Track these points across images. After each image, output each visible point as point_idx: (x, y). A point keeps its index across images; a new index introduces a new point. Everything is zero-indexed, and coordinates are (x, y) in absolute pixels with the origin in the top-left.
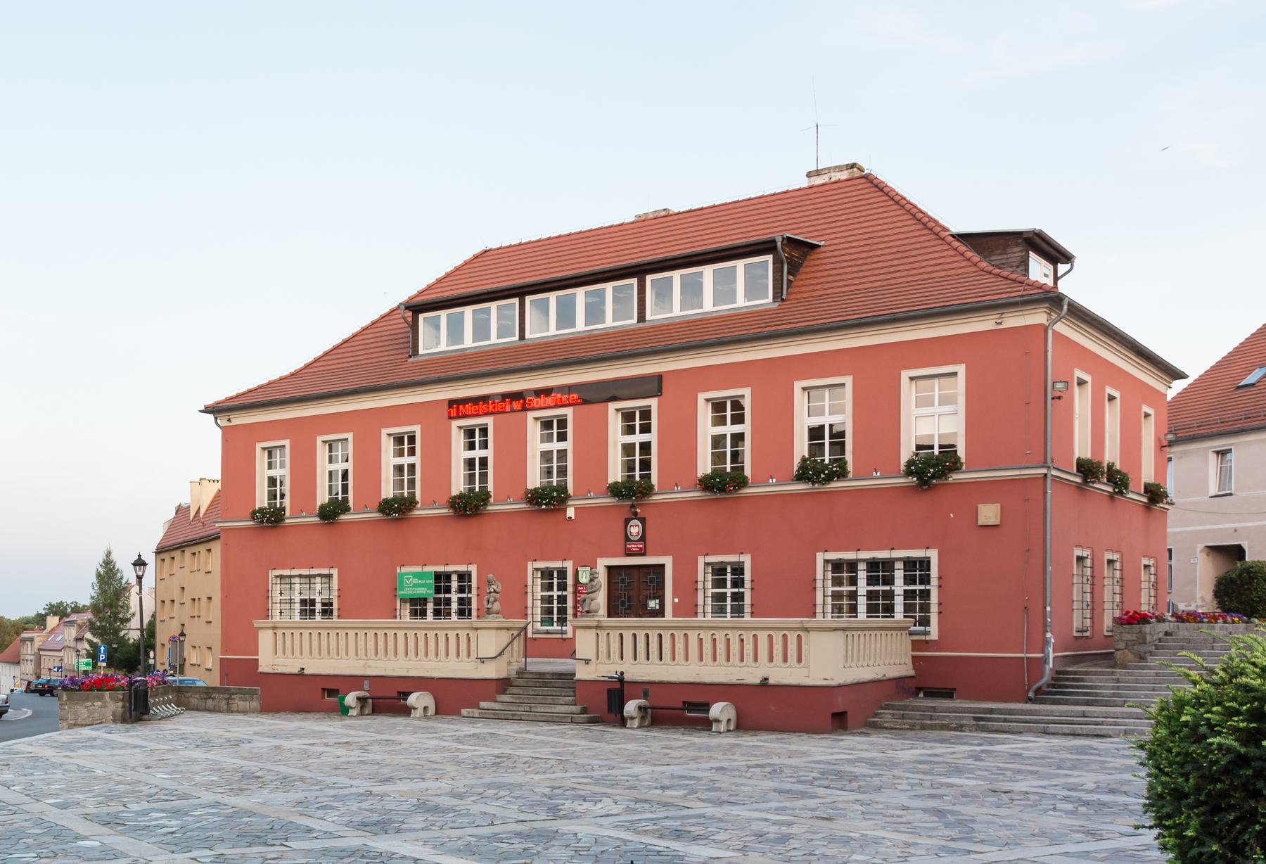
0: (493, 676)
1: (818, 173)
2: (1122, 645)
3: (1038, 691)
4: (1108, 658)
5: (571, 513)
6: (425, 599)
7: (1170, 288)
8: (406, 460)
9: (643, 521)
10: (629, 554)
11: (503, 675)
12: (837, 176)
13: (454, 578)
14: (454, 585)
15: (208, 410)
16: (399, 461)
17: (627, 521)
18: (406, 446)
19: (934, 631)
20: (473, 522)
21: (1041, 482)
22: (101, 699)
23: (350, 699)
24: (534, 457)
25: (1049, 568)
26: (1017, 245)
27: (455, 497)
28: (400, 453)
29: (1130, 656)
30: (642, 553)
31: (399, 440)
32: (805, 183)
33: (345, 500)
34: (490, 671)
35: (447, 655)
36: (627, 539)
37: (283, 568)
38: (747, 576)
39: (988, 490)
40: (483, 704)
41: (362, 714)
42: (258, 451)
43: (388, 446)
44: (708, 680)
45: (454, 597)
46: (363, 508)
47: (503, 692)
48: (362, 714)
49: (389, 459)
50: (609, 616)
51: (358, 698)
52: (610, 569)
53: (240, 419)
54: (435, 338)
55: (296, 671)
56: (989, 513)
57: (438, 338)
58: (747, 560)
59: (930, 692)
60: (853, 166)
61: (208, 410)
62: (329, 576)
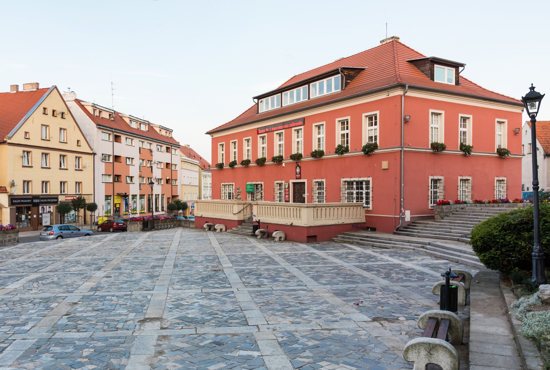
0: (237, 219)
1: (383, 41)
2: (437, 213)
3: (397, 230)
4: (432, 218)
5: (284, 165)
6: (136, 195)
7: (499, 70)
8: (345, 132)
9: (300, 167)
10: (297, 178)
11: (242, 219)
12: (388, 41)
13: (355, 183)
14: (364, 186)
15: (207, 133)
16: (343, 132)
17: (296, 167)
18: (346, 126)
19: (370, 206)
20: (263, 167)
21: (399, 153)
22: (137, 224)
23: (205, 226)
24: (276, 146)
25: (403, 185)
26: (428, 63)
27: (313, 152)
28: (343, 129)
29: (439, 217)
30: (300, 178)
31: (370, 118)
32: (380, 44)
33: (347, 147)
34: (236, 218)
35: (321, 217)
36: (296, 174)
37: (317, 178)
38: (371, 186)
39: (384, 156)
40: (233, 229)
41: (261, 238)
42: (314, 127)
43: (338, 126)
44: (280, 223)
45: (364, 191)
46: (329, 153)
47: (241, 225)
48: (261, 238)
49: (339, 131)
50: (294, 202)
51: (261, 232)
52: (294, 183)
53: (216, 136)
54: (265, 107)
55: (289, 224)
56: (385, 165)
57: (316, 93)
58: (370, 179)
59: (366, 229)
60: (393, 37)
61: (207, 133)
62: (233, 185)
